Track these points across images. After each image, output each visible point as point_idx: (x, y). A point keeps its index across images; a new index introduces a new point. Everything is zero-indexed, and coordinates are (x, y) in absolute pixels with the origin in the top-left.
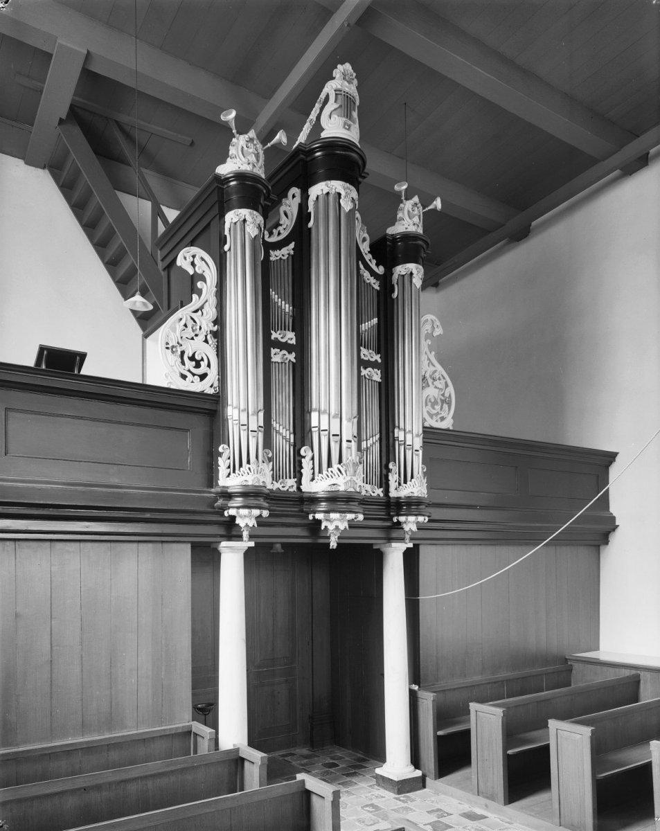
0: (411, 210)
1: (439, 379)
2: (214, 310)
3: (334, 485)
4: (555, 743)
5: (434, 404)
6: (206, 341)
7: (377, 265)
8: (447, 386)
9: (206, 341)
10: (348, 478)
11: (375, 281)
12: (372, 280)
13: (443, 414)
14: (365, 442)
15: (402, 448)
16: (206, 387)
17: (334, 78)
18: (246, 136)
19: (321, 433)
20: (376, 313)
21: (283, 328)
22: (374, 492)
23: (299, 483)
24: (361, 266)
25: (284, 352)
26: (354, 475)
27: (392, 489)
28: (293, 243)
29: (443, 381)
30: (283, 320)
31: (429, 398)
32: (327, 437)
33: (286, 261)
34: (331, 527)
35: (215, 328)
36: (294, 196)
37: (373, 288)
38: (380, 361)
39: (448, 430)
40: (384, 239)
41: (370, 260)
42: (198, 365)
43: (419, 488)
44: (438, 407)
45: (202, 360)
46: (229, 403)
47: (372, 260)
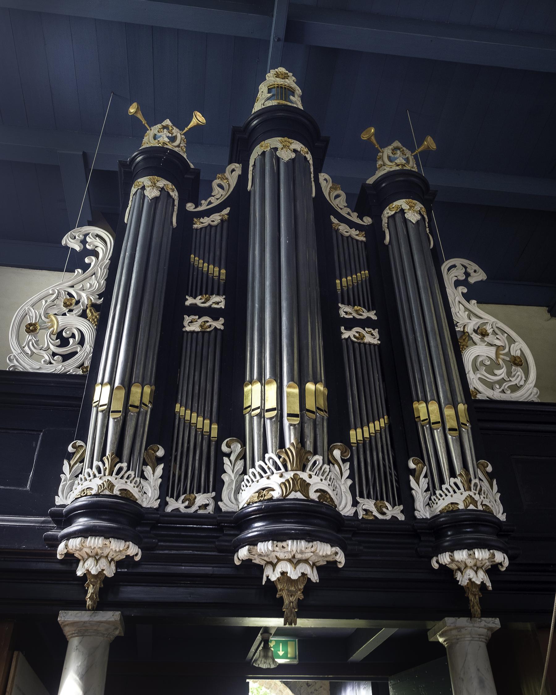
0: (391, 155)
3: (264, 489)
5: (490, 370)
7: (361, 217)
8: (511, 341)
9: (84, 315)
10: (289, 475)
11: (358, 232)
12: (354, 233)
13: (514, 381)
14: (257, 387)
15: (438, 434)
20: (197, 168)
22: (383, 514)
23: (218, 498)
26: (303, 469)
27: (420, 504)
28: (228, 209)
30: (195, 277)
31: (480, 359)
33: (219, 229)
34: (496, 620)
36: (233, 170)
37: (357, 241)
38: (375, 318)
39: (532, 403)
40: (365, 187)
41: (349, 214)
42: (64, 342)
43: (466, 494)
44: (501, 373)
45: (73, 336)
47: (351, 214)
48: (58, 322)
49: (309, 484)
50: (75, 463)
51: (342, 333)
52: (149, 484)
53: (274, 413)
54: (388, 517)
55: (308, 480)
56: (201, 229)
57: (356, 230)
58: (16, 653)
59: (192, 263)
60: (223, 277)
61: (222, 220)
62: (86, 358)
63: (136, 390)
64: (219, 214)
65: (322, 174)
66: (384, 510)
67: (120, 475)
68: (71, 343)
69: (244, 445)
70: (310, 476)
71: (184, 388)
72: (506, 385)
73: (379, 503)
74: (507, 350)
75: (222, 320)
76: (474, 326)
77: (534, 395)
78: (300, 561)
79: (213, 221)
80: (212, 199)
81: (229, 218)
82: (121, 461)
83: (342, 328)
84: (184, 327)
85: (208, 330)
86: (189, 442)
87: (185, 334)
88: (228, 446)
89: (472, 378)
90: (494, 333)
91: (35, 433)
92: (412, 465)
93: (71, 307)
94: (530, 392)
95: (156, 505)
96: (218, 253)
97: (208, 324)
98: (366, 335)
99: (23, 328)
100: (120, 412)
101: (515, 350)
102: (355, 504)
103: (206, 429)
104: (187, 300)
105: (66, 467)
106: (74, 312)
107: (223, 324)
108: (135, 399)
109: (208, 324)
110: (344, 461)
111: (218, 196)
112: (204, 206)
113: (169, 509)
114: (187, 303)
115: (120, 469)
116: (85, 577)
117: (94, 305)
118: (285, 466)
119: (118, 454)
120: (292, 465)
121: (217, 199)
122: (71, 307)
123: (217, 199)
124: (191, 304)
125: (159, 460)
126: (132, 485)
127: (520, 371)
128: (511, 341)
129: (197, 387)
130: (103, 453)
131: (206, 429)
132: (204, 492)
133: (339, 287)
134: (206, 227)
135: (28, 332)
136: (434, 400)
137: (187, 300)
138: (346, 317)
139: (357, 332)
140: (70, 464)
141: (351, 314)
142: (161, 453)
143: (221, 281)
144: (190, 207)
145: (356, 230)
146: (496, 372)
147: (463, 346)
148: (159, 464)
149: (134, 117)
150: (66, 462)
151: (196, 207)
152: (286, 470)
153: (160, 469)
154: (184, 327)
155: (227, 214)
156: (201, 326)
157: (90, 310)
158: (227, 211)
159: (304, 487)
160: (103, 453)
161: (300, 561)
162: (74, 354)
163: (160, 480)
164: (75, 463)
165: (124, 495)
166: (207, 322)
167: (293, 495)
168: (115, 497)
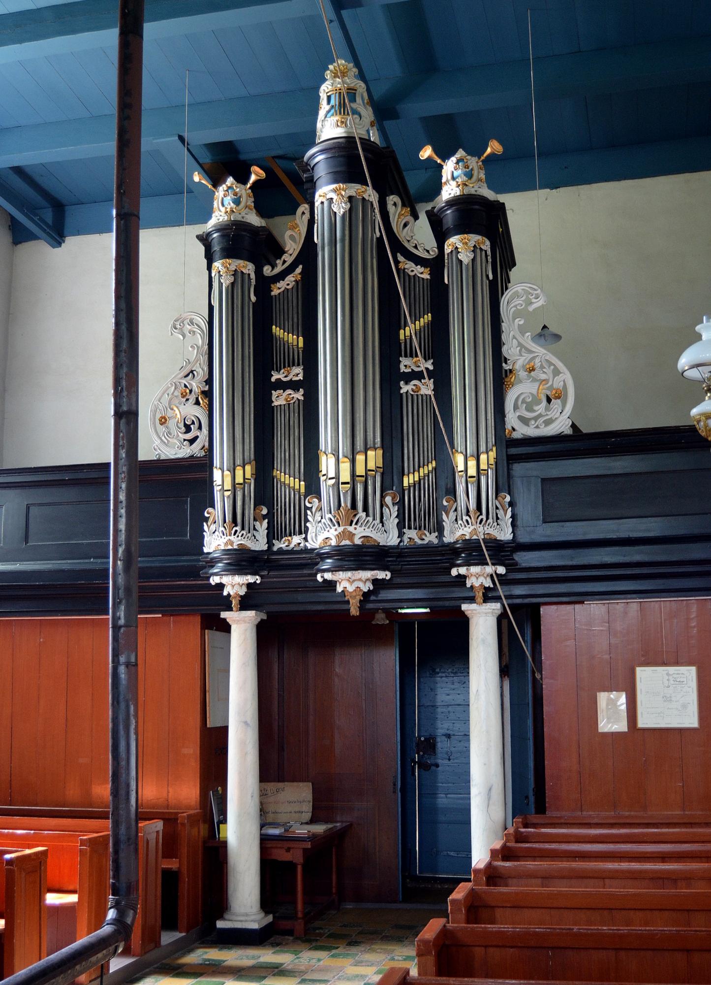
1: (542, 367)
2: (504, 329)
3: (327, 538)
4: (142, 751)
6: (197, 403)
9: (197, 403)
10: (341, 529)
11: (422, 269)
13: (551, 415)
16: (196, 450)
17: (327, 80)
18: (224, 186)
19: (469, 479)
21: (287, 365)
24: (401, 258)
25: (289, 391)
28: (301, 266)
29: (549, 370)
32: (475, 484)
35: (207, 388)
36: (303, 213)
44: (541, 408)
45: (193, 423)
46: (215, 465)
48: (180, 413)
49: (354, 534)
50: (211, 524)
51: (401, 388)
52: (259, 534)
53: (333, 481)
54: (425, 542)
55: (354, 532)
56: (279, 294)
57: (421, 267)
58: (206, 631)
59: (274, 334)
60: (301, 344)
61: (296, 281)
62: (205, 441)
63: (239, 472)
64: (292, 275)
65: (391, 197)
66: (424, 537)
67: (237, 535)
68: (193, 428)
69: (320, 500)
70: (355, 529)
71: (279, 456)
72: (541, 420)
73: (420, 533)
74: (550, 383)
75: (302, 391)
76: (524, 361)
77: (566, 426)
78: (354, 581)
79: (288, 285)
80: (284, 257)
81: (301, 278)
82: (236, 526)
83: (402, 383)
84: (273, 402)
85: (292, 402)
86: (285, 499)
87: (275, 407)
88: (310, 503)
89: (510, 417)
90: (542, 367)
91: (185, 499)
92: (445, 503)
93: (187, 397)
94: (562, 423)
95: (265, 547)
96: (295, 320)
97: (292, 396)
98: (422, 387)
99: (157, 421)
100: (229, 490)
101: (558, 383)
102: (401, 535)
103: (297, 487)
104: (272, 375)
105: (206, 527)
106: (190, 401)
107: (303, 395)
108: (239, 479)
109: (292, 396)
110: (394, 504)
111: (290, 252)
112: (279, 269)
113: (275, 549)
114: (273, 379)
115: (236, 531)
116: (229, 595)
117: (203, 392)
118: (338, 523)
119: (234, 521)
120: (342, 523)
121: (291, 255)
122: (187, 397)
123: (291, 255)
124: (276, 380)
125: (264, 517)
126: (246, 539)
127: (558, 405)
128: (557, 372)
129: (287, 454)
130: (225, 522)
131: (297, 487)
132: (299, 535)
133: (402, 337)
134: (283, 291)
135: (161, 424)
136: (462, 453)
137: (272, 375)
138: (406, 371)
139: (414, 385)
140: (208, 525)
141: (410, 367)
142: (265, 511)
143: (237, 486)
144: (267, 270)
145: (421, 267)
146: (536, 408)
147: (509, 385)
148: (264, 519)
149: (200, 182)
150: (205, 524)
151: (273, 268)
152: (339, 526)
153: (265, 523)
154: (273, 402)
155: (300, 274)
156: (286, 400)
157: (201, 398)
158: (299, 269)
159: (351, 536)
160: (225, 522)
161: (354, 581)
162: (196, 438)
163: (266, 531)
164: (211, 524)
165: (241, 548)
166: (290, 394)
167: (343, 543)
168: (235, 550)
